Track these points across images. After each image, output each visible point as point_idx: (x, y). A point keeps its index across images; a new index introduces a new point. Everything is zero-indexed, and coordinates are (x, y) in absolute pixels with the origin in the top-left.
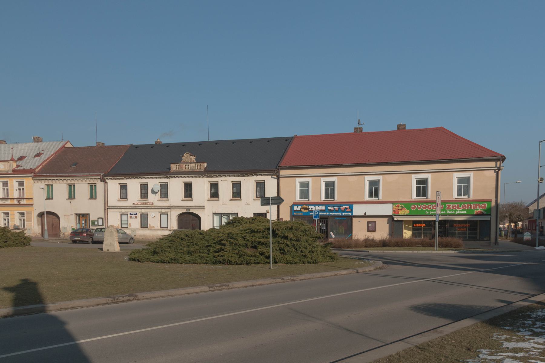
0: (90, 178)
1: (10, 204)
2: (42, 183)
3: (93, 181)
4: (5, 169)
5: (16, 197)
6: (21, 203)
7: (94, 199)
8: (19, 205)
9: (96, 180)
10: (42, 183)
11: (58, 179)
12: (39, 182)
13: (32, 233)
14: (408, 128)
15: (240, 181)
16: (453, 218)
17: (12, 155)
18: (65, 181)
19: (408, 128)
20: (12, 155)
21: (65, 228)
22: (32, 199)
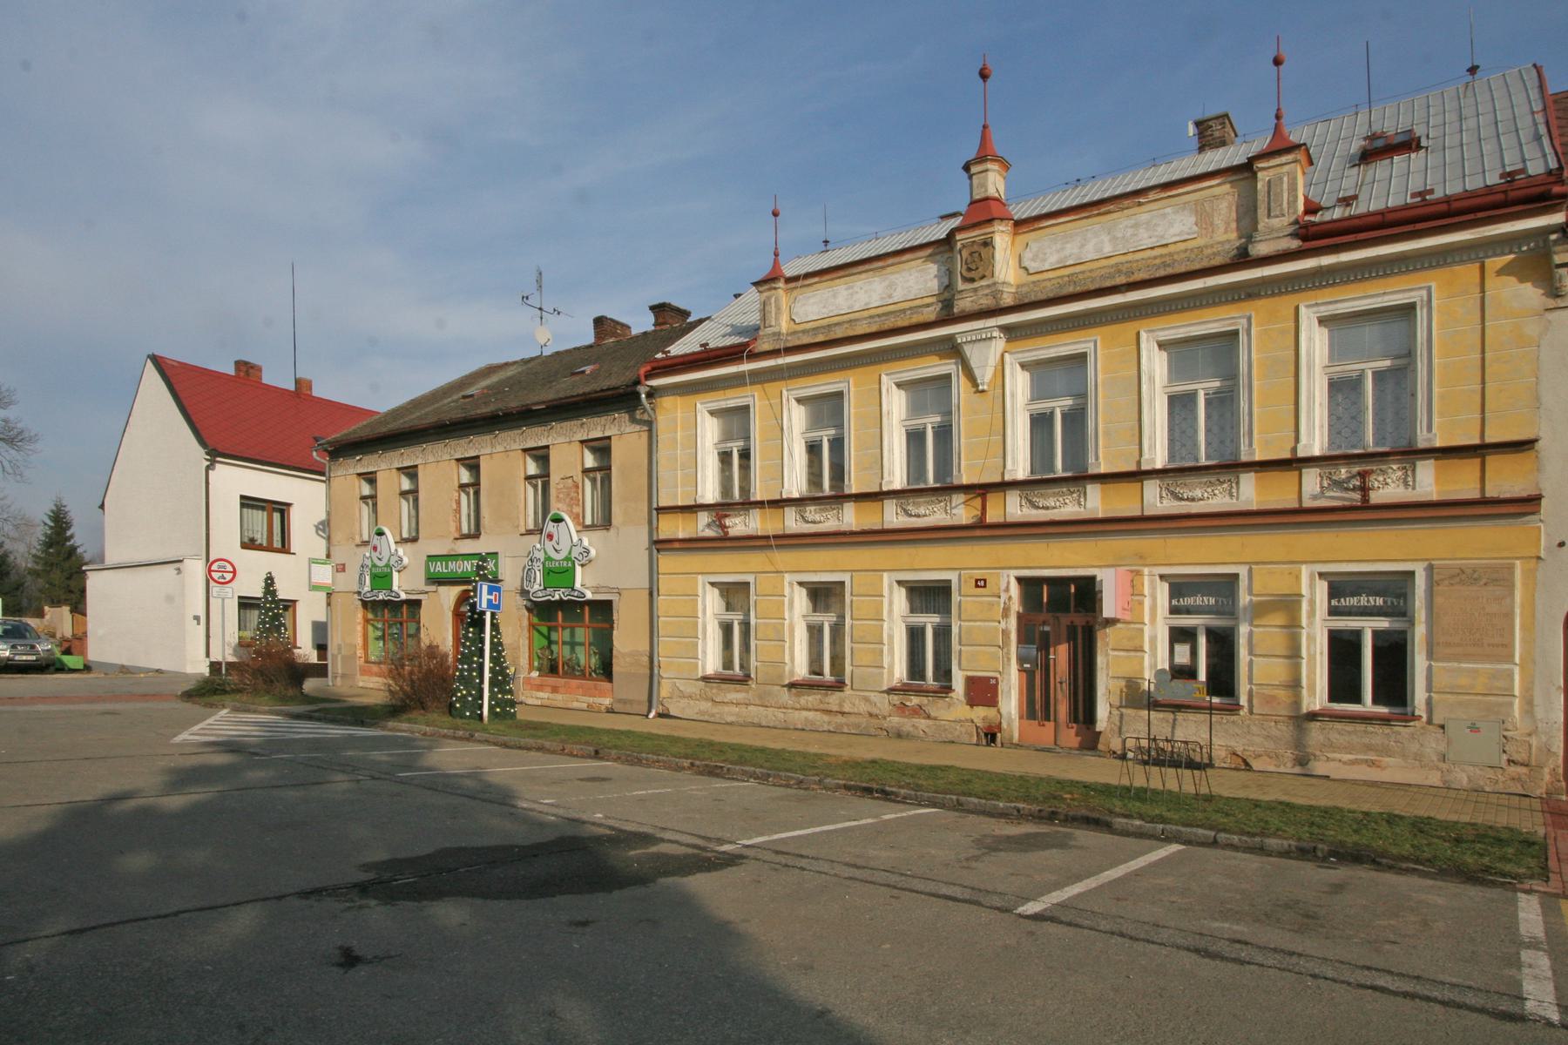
4: (1200, 242)
6: (1376, 497)
8: (724, 542)
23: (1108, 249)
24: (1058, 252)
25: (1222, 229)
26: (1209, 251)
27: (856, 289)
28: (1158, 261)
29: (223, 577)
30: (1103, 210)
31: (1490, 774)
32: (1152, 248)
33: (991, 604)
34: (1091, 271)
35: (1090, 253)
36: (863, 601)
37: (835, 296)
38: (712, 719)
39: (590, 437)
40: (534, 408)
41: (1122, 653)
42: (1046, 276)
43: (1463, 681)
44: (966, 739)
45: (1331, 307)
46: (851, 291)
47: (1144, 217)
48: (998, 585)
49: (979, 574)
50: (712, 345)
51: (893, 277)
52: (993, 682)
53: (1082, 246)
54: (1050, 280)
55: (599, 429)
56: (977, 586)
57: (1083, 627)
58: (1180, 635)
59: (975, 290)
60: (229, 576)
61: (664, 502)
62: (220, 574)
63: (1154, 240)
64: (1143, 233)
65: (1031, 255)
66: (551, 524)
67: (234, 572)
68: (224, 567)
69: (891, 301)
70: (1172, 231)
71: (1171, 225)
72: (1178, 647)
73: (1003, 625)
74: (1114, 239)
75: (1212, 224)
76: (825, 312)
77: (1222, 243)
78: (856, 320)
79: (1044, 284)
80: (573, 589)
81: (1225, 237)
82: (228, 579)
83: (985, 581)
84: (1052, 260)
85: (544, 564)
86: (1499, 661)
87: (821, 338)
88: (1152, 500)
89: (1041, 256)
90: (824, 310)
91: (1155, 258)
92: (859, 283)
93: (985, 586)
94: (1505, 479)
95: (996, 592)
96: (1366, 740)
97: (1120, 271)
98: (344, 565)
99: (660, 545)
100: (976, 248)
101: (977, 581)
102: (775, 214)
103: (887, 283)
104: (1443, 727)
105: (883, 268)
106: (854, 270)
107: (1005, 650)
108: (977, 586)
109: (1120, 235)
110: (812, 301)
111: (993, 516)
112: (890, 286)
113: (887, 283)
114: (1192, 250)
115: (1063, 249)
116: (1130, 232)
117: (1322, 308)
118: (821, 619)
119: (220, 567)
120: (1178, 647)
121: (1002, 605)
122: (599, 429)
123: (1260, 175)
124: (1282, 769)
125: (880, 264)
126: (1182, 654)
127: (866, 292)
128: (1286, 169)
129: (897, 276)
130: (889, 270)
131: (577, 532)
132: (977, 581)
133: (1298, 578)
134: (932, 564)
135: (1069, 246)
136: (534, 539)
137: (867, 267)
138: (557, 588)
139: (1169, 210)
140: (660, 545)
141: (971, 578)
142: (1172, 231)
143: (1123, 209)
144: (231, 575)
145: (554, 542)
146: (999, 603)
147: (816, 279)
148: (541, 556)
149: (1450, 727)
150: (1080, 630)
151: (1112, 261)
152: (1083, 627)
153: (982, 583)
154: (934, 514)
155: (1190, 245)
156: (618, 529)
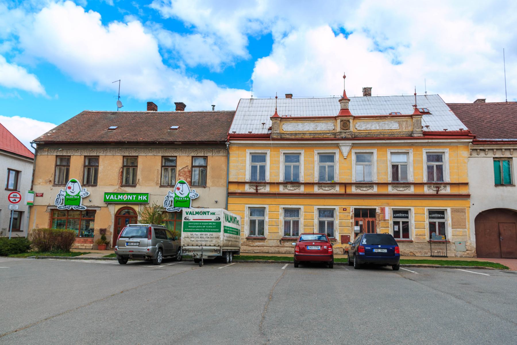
0: (495, 148)
1: (376, 193)
2: (487, 156)
3: (476, 153)
4: (400, 130)
5: (247, 181)
6: (259, 191)
7: (92, 186)
8: (257, 194)
9: (475, 151)
10: (487, 156)
11: (509, 148)
12: (482, 154)
13: (467, 250)
14: (487, 101)
15: (9, 170)
16: (253, 218)
17: (276, 109)
18: (491, 154)
19: (487, 101)
20: (276, 109)
21: (460, 243)
22: (467, 184)
23: (378, 128)
24: (365, 126)
25: (404, 128)
26: (402, 133)
27: (305, 125)
28: (390, 133)
29: (15, 200)
30: (377, 118)
31: (463, 253)
32: (388, 130)
33: (348, 215)
34: (374, 132)
35: (373, 128)
36: (307, 214)
37: (298, 125)
38: (249, 252)
39: (198, 155)
40: (175, 143)
41: (383, 228)
42: (362, 131)
43: (458, 233)
44: (340, 253)
45: (429, 150)
46: (303, 125)
47: (387, 122)
48: (350, 210)
49: (344, 207)
50: (253, 133)
51: (317, 124)
52: (348, 236)
53: (371, 126)
54: (363, 133)
55: (161, 153)
56: (344, 210)
57: (372, 221)
58: (396, 223)
59: (345, 132)
60: (17, 200)
61: (231, 180)
62: (14, 199)
63: (389, 128)
64: (386, 126)
65: (358, 126)
66: (71, 183)
67: (20, 198)
68: (16, 196)
69: (316, 130)
70: (393, 127)
71: (393, 125)
72: (395, 226)
73: (351, 221)
74: (379, 126)
75: (402, 127)
76: (294, 129)
77: (405, 132)
78: (305, 133)
79: (362, 133)
80: (79, 206)
81: (405, 131)
82: (17, 201)
83: (346, 209)
84: (363, 128)
85: (65, 197)
86: (464, 229)
87: (293, 137)
88: (390, 190)
89: (360, 126)
90: (294, 129)
91: (390, 132)
92: (306, 123)
93: (346, 210)
94: (463, 191)
95: (349, 212)
96: (439, 247)
97: (381, 134)
98: (43, 194)
99: (230, 194)
100: (345, 122)
101: (344, 209)
102: (119, 97)
103: (315, 125)
104: (454, 243)
105: (314, 121)
106: (307, 119)
107: (352, 228)
108: (344, 210)
109: (381, 125)
110: (290, 125)
111: (348, 191)
112: (316, 126)
113: (315, 125)
114: (398, 132)
115: (366, 126)
116: (383, 125)
117: (427, 150)
118: (290, 219)
119: (14, 196)
120: (395, 226)
121: (351, 216)
122: (161, 153)
123: (414, 119)
124: (422, 255)
125: (313, 119)
126: (396, 229)
127: (308, 126)
128: (419, 119)
129: (318, 123)
130: (316, 121)
131: (82, 186)
132: (344, 209)
133: (424, 210)
135: (368, 125)
136: (169, 189)
137: (309, 119)
138: (70, 205)
139: (392, 122)
140: (230, 194)
141: (342, 208)
142: (393, 127)
143: (381, 119)
144: (19, 199)
145: (180, 191)
146: (350, 215)
147: (292, 120)
148: (65, 194)
149: (456, 243)
150: (371, 222)
151: (379, 131)
152: (372, 221)
153: (345, 210)
154: (290, 189)
155: (397, 131)
156: (209, 188)
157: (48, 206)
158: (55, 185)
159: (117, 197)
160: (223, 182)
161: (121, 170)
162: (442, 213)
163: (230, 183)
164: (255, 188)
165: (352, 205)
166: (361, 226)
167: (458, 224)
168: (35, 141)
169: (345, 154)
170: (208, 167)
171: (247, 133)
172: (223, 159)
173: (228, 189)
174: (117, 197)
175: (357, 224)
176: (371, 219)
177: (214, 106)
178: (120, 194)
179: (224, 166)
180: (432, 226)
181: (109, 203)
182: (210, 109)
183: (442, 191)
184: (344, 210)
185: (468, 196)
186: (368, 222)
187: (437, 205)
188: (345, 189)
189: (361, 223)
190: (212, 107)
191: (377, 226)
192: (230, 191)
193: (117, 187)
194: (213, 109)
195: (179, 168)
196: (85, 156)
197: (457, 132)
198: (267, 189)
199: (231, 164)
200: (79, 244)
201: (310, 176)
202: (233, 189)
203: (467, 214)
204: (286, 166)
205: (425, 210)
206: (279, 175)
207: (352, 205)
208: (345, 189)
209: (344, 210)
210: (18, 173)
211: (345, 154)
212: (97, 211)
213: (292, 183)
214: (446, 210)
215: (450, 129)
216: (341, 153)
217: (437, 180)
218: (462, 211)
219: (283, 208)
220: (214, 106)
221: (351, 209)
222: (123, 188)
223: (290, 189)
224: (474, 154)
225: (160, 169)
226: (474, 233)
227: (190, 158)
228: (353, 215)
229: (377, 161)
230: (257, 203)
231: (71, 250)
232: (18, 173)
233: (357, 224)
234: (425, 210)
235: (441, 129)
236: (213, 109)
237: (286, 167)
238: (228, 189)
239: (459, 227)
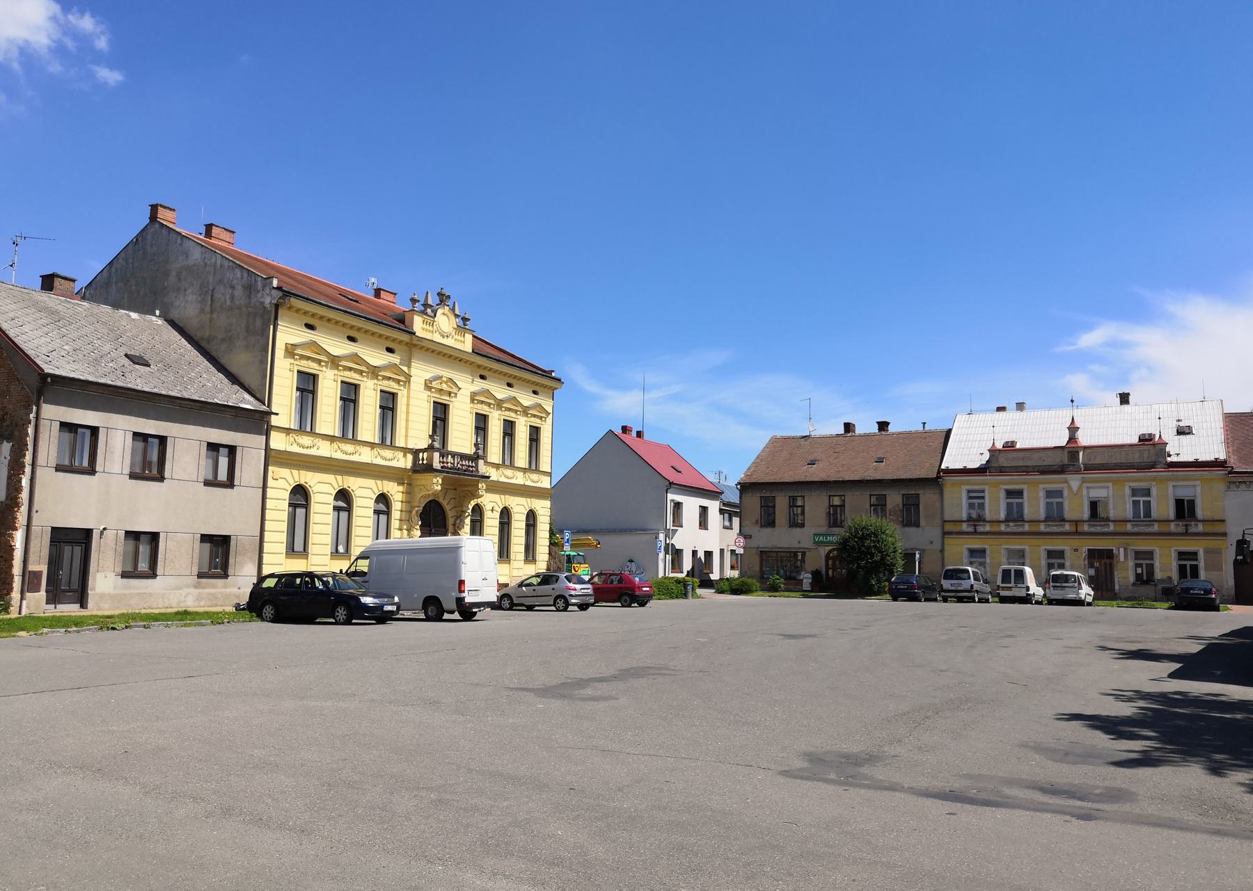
12: (1243, 486)
22: (1224, 521)
72: (1140, 572)
94: (1218, 528)
133: (1170, 551)
134: (1143, 545)
157: (757, 548)
158: (762, 526)
159: (826, 539)
160: (938, 522)
161: (828, 510)
162: (1193, 555)
163: (945, 521)
164: (973, 527)
165: (1086, 545)
166: (1097, 570)
167: (1214, 566)
168: (739, 483)
169: (1075, 488)
170: (921, 506)
171: (962, 467)
172: (937, 497)
173: (943, 528)
174: (826, 539)
175: (1091, 565)
176: (1108, 561)
177: (925, 423)
178: (830, 535)
179: (938, 504)
180: (1182, 569)
181: (818, 544)
182: (920, 428)
183: (980, 529)
184: (1076, 550)
185: (1225, 534)
186: (1105, 563)
187: (1188, 546)
188: (1077, 527)
189: (1096, 564)
190: (922, 425)
191: (1115, 569)
192: (945, 530)
193: (825, 528)
194: (924, 427)
195: (889, 507)
196: (790, 497)
197: (1212, 462)
198: (988, 528)
199: (946, 503)
200: (792, 587)
201: (185, 597)
202: (948, 527)
203: (1223, 556)
204: (1008, 503)
205: (1173, 551)
206: (999, 513)
207: (1086, 545)
208: (1077, 527)
209: (1076, 550)
210: (232, 450)
211: (1075, 488)
212: (807, 553)
213: (1014, 521)
214: (1198, 550)
215: (1202, 458)
216: (1070, 487)
217: (1144, 518)
218: (1218, 552)
219: (1006, 549)
220: (925, 423)
221: (1084, 551)
222: (832, 529)
223: (1012, 527)
224: (1233, 487)
225: (869, 508)
226: (1233, 576)
227: (901, 496)
228: (1087, 557)
229: (1113, 496)
230: (976, 544)
231: (810, 576)
232: (232, 450)
233: (1091, 565)
234: (1173, 551)
235: (1191, 459)
236: (924, 427)
237: (1008, 504)
238: (943, 528)
239: (349, 472)
